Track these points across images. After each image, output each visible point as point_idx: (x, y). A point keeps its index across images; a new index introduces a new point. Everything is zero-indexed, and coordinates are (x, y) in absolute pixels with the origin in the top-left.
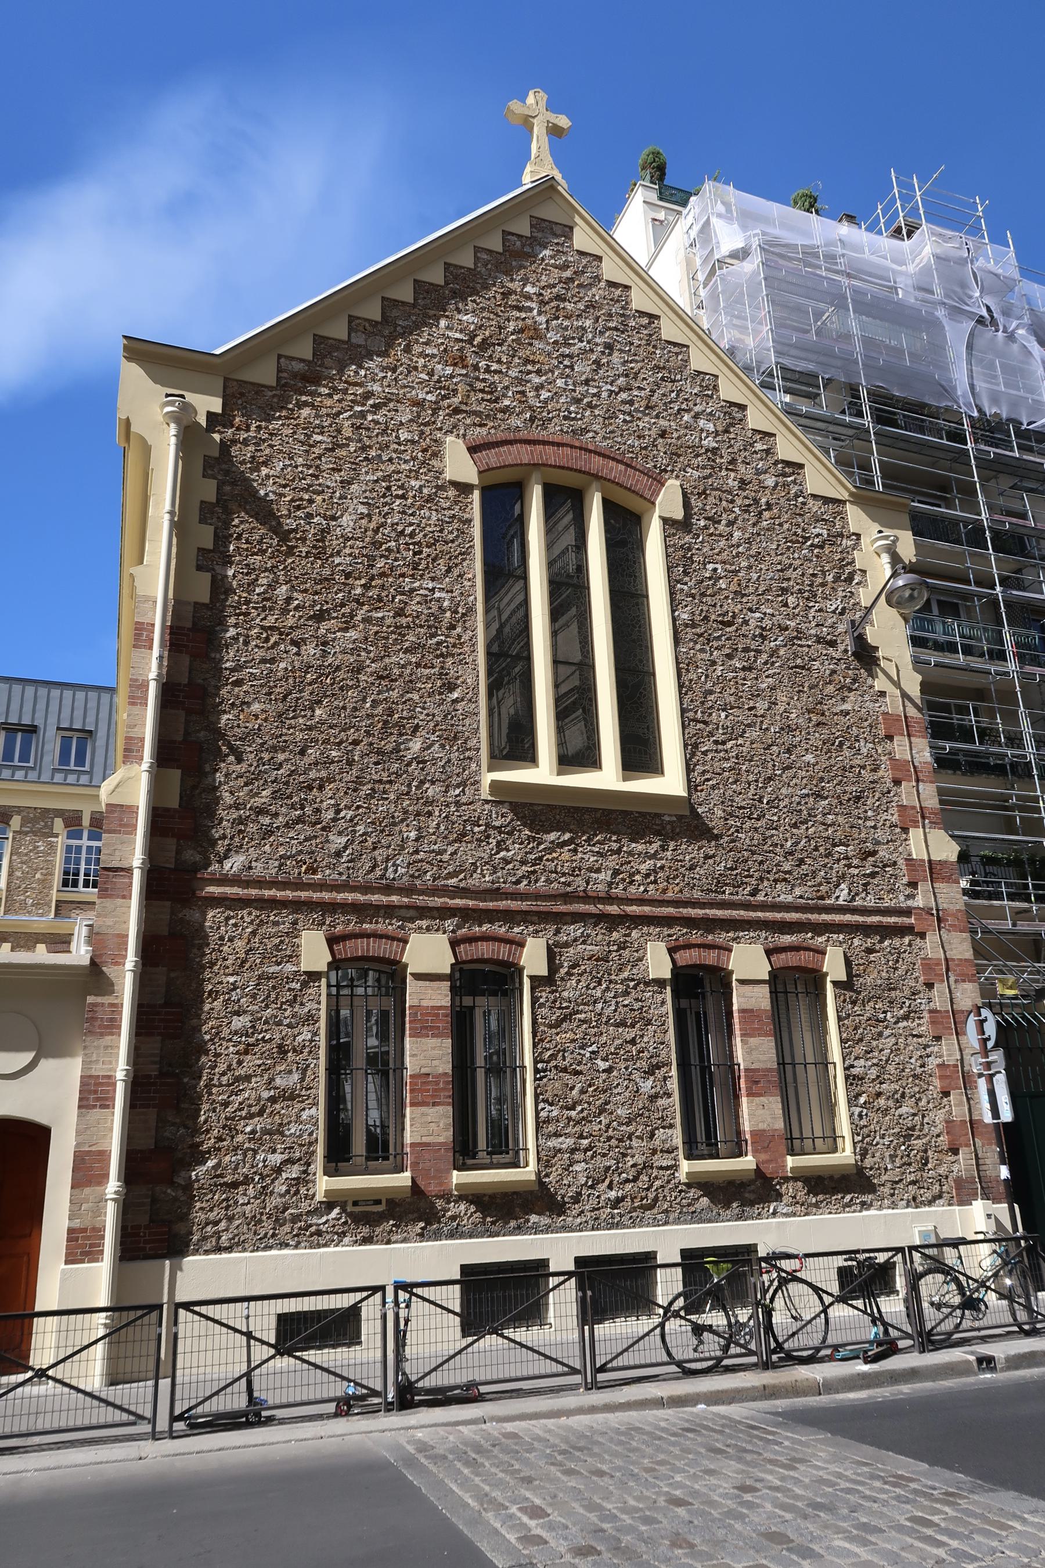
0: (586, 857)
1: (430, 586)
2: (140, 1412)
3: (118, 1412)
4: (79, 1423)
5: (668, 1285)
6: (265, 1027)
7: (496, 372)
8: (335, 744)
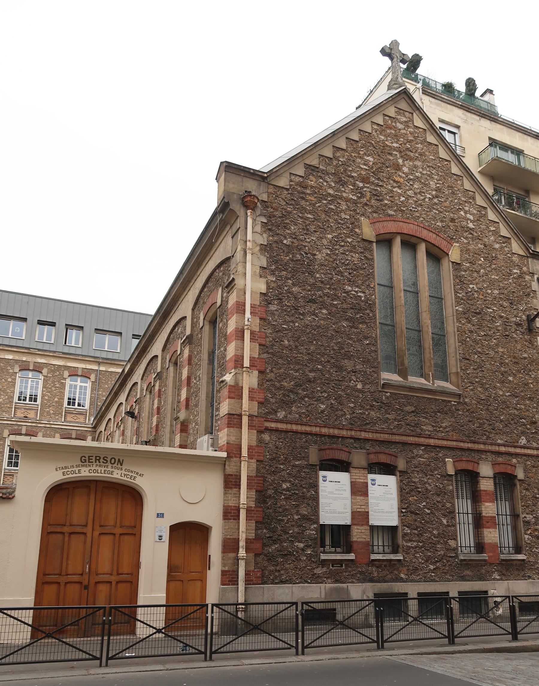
1: (357, 289)
2: (291, 644)
5: (413, 606)
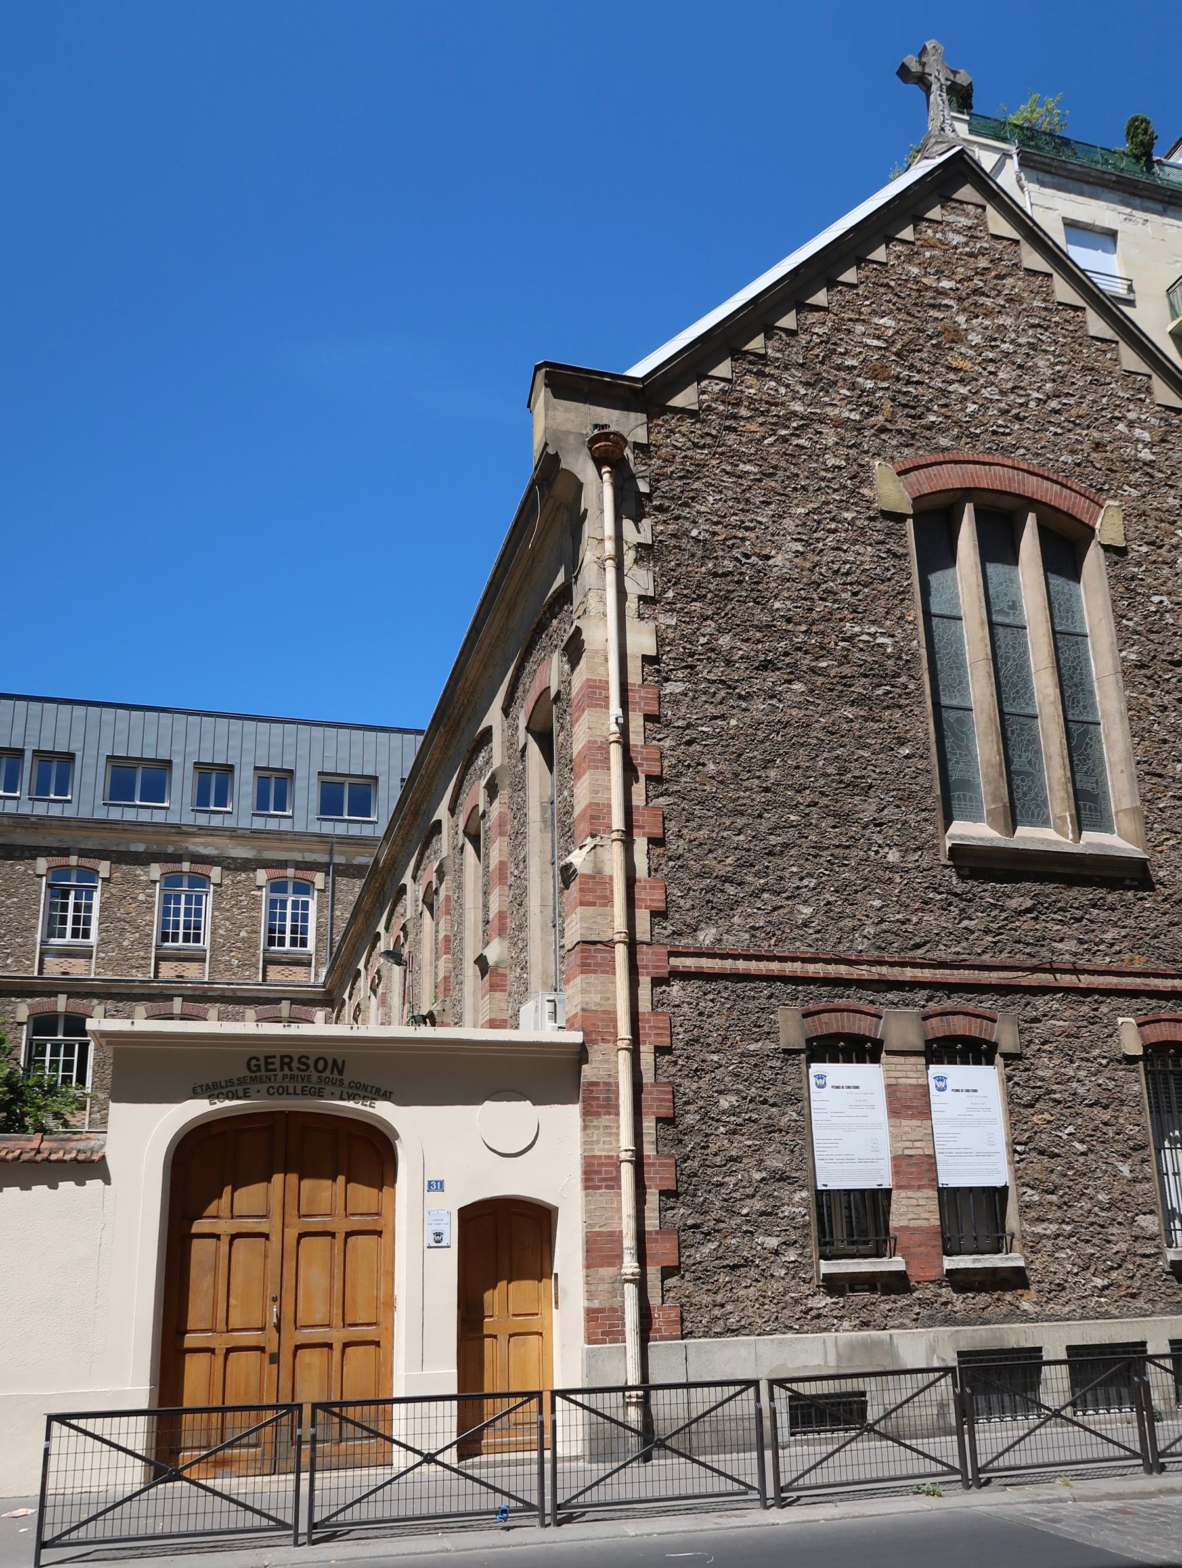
0: (1049, 925)
1: (873, 630)
3: (257, 1517)
4: (663, 1494)
5: (1055, 1385)
6: (751, 1106)
7: (918, 383)
8: (791, 807)
